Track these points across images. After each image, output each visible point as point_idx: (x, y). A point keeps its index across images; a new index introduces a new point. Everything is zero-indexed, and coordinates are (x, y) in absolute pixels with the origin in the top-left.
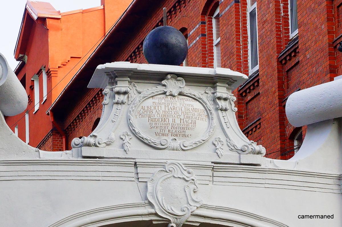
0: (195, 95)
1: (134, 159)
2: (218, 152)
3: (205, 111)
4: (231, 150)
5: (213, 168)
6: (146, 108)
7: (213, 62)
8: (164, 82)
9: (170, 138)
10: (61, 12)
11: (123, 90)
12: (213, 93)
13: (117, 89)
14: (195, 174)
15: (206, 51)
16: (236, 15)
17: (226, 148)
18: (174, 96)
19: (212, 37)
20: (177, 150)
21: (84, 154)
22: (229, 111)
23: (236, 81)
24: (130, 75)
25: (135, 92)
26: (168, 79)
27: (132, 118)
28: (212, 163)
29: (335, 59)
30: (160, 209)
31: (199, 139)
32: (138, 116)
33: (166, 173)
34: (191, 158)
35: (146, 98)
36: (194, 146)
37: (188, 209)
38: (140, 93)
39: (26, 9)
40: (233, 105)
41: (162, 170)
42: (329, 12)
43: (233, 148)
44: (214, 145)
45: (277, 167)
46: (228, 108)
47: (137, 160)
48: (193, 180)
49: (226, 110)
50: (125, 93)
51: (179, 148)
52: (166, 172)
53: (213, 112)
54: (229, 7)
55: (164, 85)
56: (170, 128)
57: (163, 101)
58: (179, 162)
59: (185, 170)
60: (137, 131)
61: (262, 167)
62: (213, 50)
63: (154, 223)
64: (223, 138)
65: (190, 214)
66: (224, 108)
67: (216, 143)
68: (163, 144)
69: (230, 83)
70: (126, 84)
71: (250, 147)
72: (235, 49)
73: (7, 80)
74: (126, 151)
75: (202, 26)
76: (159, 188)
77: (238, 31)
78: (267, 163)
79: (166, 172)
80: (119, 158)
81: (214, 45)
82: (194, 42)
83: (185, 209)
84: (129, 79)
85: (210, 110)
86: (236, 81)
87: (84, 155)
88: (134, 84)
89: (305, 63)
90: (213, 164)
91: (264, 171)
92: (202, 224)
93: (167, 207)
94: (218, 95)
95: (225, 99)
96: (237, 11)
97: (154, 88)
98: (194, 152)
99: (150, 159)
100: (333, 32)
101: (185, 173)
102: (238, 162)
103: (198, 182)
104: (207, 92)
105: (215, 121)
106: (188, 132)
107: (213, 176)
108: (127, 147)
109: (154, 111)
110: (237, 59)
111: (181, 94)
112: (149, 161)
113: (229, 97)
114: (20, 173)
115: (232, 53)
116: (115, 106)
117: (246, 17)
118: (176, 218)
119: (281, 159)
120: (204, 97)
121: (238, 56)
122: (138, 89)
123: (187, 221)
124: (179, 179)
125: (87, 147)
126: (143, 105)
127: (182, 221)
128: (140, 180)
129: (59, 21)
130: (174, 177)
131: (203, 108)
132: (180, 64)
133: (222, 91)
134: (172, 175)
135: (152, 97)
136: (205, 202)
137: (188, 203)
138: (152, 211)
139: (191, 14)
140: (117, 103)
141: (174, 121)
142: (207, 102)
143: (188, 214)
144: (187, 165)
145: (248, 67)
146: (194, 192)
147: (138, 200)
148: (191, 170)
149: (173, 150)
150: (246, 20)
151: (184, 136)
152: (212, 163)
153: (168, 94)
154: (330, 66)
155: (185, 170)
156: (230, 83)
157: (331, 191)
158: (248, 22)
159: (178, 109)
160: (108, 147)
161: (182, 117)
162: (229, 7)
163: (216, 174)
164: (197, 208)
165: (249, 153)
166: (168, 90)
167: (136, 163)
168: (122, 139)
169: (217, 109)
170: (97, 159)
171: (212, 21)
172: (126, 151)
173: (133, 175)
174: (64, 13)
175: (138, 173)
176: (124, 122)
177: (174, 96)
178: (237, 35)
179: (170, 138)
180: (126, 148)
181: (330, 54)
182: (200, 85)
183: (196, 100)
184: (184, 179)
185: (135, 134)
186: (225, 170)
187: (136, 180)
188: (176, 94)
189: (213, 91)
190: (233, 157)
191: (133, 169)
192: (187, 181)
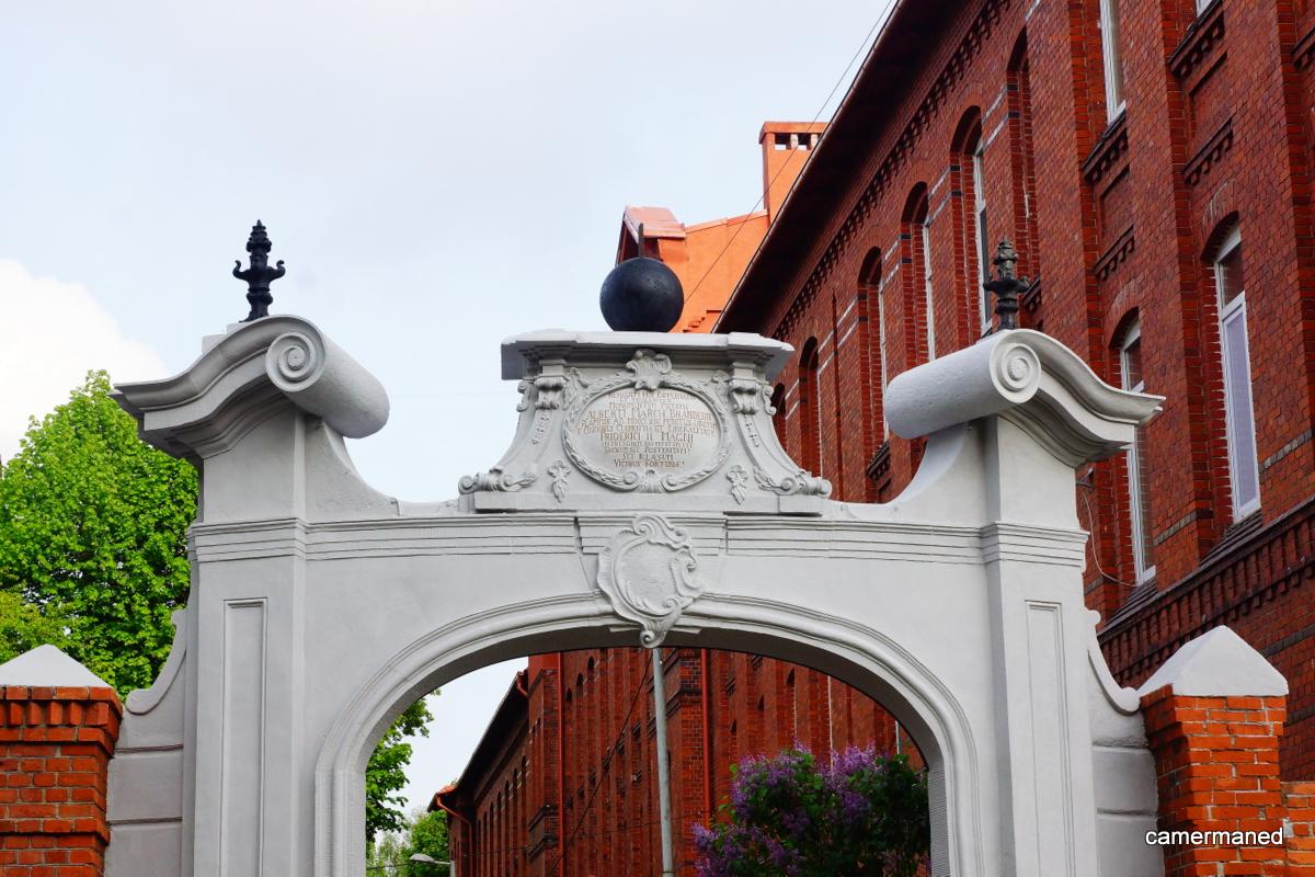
0: (691, 387)
1: (575, 511)
2: (735, 492)
3: (712, 417)
4: (763, 488)
5: (726, 524)
6: (597, 416)
7: (925, 312)
8: (630, 365)
9: (641, 472)
10: (686, 226)
11: (553, 382)
12: (728, 382)
13: (540, 381)
14: (691, 536)
15: (912, 291)
16: (954, 219)
17: (752, 484)
18: (650, 390)
19: (923, 263)
20: (655, 492)
21: (479, 506)
22: (760, 415)
23: (772, 356)
24: (565, 353)
25: (577, 385)
26: (638, 359)
27: (570, 435)
28: (725, 513)
29: (1099, 298)
30: (621, 602)
31: (700, 469)
32: (582, 431)
33: (634, 537)
34: (682, 505)
35: (598, 396)
36: (690, 483)
37: (676, 603)
38: (585, 386)
39: (624, 224)
40: (768, 402)
41: (626, 531)
42: (1086, 210)
43: (765, 484)
44: (730, 479)
45: (854, 517)
46: (756, 408)
47: (578, 514)
48: (687, 547)
49: (752, 412)
50: (557, 388)
51: (661, 489)
52: (634, 533)
53: (728, 417)
54: (943, 205)
55: (631, 371)
56: (642, 450)
57: (630, 400)
58: (659, 514)
59: (672, 530)
60: (579, 459)
61: (824, 518)
62: (925, 288)
63: (612, 630)
64: (747, 467)
65: (681, 611)
66: (749, 410)
67: (732, 476)
68: (629, 481)
69: (761, 360)
70: (560, 371)
71: (798, 481)
72: (955, 286)
73: (325, 372)
74: (557, 497)
75: (903, 243)
76: (621, 564)
77: (959, 251)
78: (833, 510)
79: (634, 533)
80: (545, 511)
81: (927, 278)
82: (892, 274)
83: (671, 603)
84: (563, 361)
85: (720, 414)
86: (772, 356)
87: (478, 506)
88: (575, 371)
89: (1050, 310)
90: (726, 516)
91: (827, 526)
92: (705, 630)
93: (637, 600)
94: (736, 384)
95: (751, 392)
96: (957, 208)
97: (613, 376)
98: (689, 493)
99: (604, 510)
100: (1095, 248)
101: (672, 535)
102: (775, 511)
103: (697, 551)
104: (716, 379)
105: (731, 434)
106: (677, 457)
107: (727, 539)
108: (561, 488)
109: (612, 421)
110: (959, 304)
111: (663, 386)
112: (601, 514)
113: (758, 387)
114: (361, 545)
115: (950, 294)
116: (539, 414)
117: (973, 222)
118: (654, 621)
119: (868, 502)
120: (710, 391)
121: (961, 298)
122: (581, 379)
123: (675, 626)
124: (659, 547)
125: (485, 493)
126: (590, 409)
127: (666, 624)
128: (585, 550)
129: (683, 243)
130: (649, 542)
131: (708, 411)
132: (665, 327)
133: (744, 377)
134: (644, 539)
135: (609, 393)
136: (709, 589)
137: (677, 591)
138: (606, 608)
139: (886, 220)
140: (543, 408)
141: (650, 437)
142: (715, 398)
143: (677, 612)
144: (675, 520)
145: (979, 320)
146: (690, 570)
147: (585, 590)
148: (682, 529)
149: (649, 491)
150: (974, 229)
151: (671, 464)
152: (725, 513)
153: (637, 386)
154: (1090, 313)
155: (672, 530)
156: (761, 360)
157: (965, 560)
158: (978, 232)
159: (657, 414)
160: (524, 491)
161: (665, 430)
162: (943, 205)
163: (732, 534)
164: (695, 600)
165: (797, 493)
166: (639, 379)
167: (576, 519)
168: (551, 474)
169: (735, 412)
170: (504, 514)
171: (921, 233)
172: (557, 497)
173: (573, 541)
174: (691, 228)
175: (581, 538)
176: (555, 443)
177: (650, 390)
178: (957, 258)
179: (641, 472)
180: (557, 491)
181: (1089, 290)
182: (702, 367)
183: (694, 395)
184: (668, 546)
185: (576, 464)
186: (751, 527)
187: (578, 552)
188: (654, 387)
189: (727, 377)
190: (767, 502)
191: (571, 531)
192: (674, 550)
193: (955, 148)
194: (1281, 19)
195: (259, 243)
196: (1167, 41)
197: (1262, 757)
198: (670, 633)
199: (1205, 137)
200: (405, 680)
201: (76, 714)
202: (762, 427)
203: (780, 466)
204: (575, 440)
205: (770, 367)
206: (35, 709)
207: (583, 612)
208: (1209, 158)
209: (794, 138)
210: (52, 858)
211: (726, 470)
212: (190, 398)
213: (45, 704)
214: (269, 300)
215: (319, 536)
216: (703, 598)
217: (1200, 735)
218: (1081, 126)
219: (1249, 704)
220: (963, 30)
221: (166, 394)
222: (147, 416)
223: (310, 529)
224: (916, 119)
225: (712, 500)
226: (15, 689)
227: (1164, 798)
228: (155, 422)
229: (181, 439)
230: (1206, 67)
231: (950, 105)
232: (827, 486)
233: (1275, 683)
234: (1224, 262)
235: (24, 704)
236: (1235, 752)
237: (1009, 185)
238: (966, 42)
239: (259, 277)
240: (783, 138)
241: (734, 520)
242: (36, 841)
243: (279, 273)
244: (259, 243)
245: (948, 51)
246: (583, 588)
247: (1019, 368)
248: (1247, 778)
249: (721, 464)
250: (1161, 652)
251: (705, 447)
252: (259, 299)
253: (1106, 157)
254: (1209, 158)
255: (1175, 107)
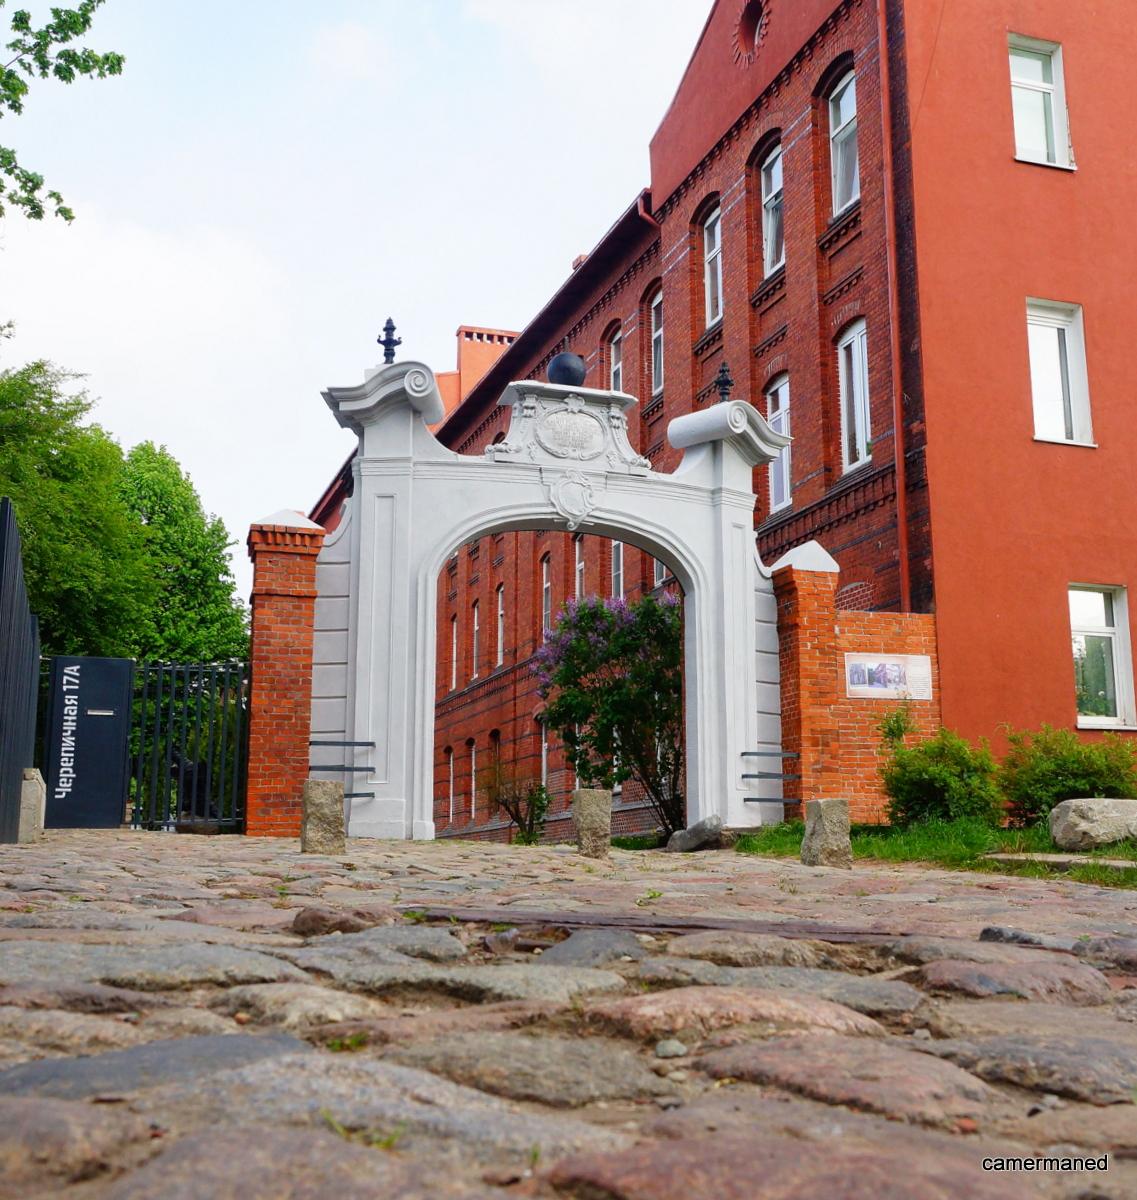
11: (531, 405)
13: (525, 404)
14: (592, 481)
31: (595, 451)
34: (591, 467)
35: (550, 414)
50: (532, 408)
78: (653, 475)
91: (649, 482)
93: (568, 508)
94: (612, 414)
95: (618, 418)
105: (610, 436)
111: (580, 411)
127: (579, 520)
133: (615, 411)
144: (584, 473)
151: (583, 448)
166: (570, 408)
179: (570, 450)
185: (540, 444)
190: (624, 469)
191: (538, 474)
193: (603, 339)
194: (819, 281)
195: (390, 328)
196: (750, 289)
197: (828, 598)
198: (581, 525)
199: (768, 335)
200: (461, 536)
201: (307, 540)
202: (622, 436)
203: (631, 454)
204: (539, 432)
205: (628, 407)
206: (288, 537)
207: (543, 511)
208: (770, 345)
209: (475, 335)
210: (295, 607)
211: (607, 452)
212: (364, 396)
213: (293, 535)
214: (393, 354)
215: (419, 467)
216: (597, 509)
217: (803, 586)
218: (693, 328)
219: (823, 575)
220: (614, 280)
221: (354, 393)
222: (341, 404)
223: (415, 464)
224: (580, 324)
225: (600, 466)
226: (279, 527)
227: (780, 615)
228: (344, 407)
229: (356, 417)
230: (770, 303)
231: (602, 318)
232: (650, 465)
233: (834, 567)
234: (771, 394)
235: (283, 534)
236: (817, 596)
237: (638, 358)
238: (615, 286)
239: (389, 344)
240: (469, 335)
241: (609, 476)
242: (288, 599)
243: (398, 343)
244: (390, 328)
245: (603, 291)
246: (542, 500)
247: (738, 418)
248: (822, 607)
249: (605, 450)
250: (783, 547)
251: (598, 442)
252: (389, 354)
253: (708, 343)
254: (770, 345)
255: (752, 320)
